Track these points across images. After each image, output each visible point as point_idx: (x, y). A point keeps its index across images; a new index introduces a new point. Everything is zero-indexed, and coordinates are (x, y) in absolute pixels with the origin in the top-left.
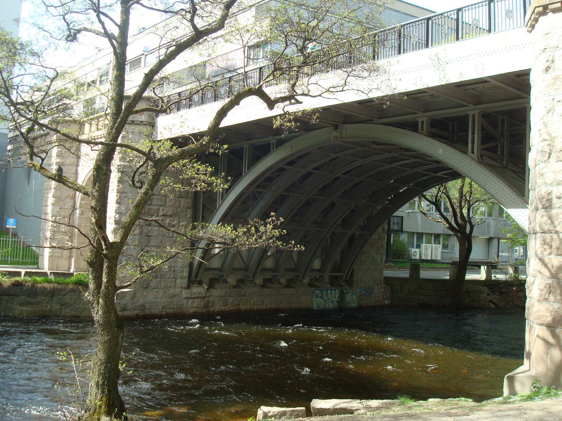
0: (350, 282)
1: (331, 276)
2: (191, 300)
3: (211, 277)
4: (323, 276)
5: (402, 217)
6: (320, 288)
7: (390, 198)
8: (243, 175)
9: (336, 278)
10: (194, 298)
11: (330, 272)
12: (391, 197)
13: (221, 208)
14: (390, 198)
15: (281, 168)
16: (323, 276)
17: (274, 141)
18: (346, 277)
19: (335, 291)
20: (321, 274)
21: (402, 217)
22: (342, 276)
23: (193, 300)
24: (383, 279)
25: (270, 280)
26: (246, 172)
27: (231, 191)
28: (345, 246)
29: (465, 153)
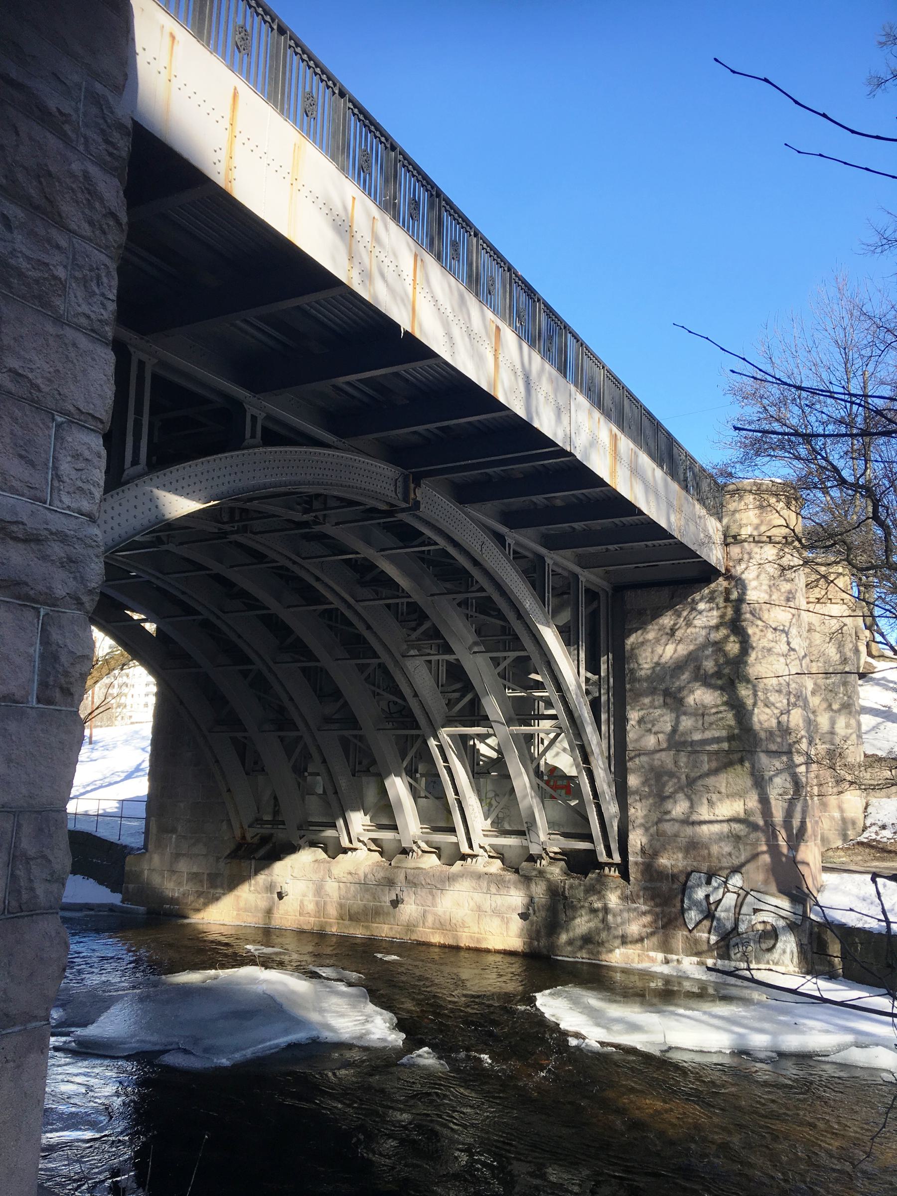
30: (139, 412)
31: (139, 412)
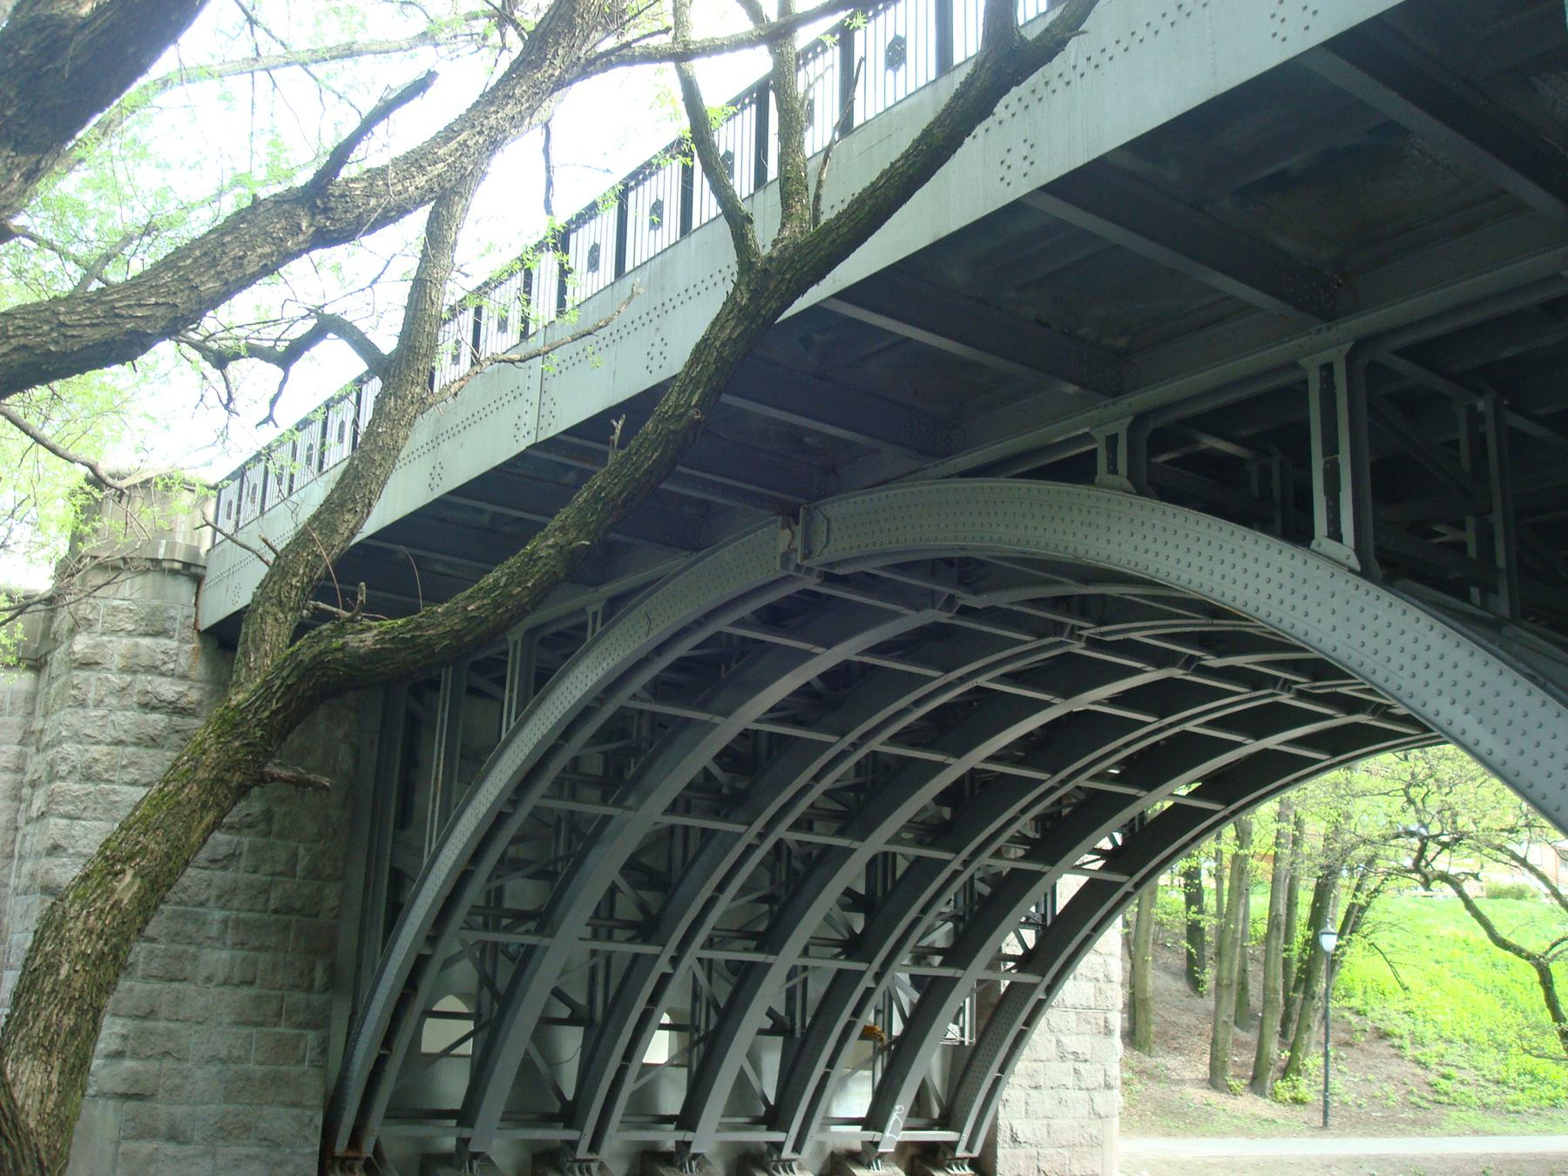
17: (598, 607)
18: (969, 1148)
22: (953, 1146)
30: (1331, 448)
31: (1331, 448)
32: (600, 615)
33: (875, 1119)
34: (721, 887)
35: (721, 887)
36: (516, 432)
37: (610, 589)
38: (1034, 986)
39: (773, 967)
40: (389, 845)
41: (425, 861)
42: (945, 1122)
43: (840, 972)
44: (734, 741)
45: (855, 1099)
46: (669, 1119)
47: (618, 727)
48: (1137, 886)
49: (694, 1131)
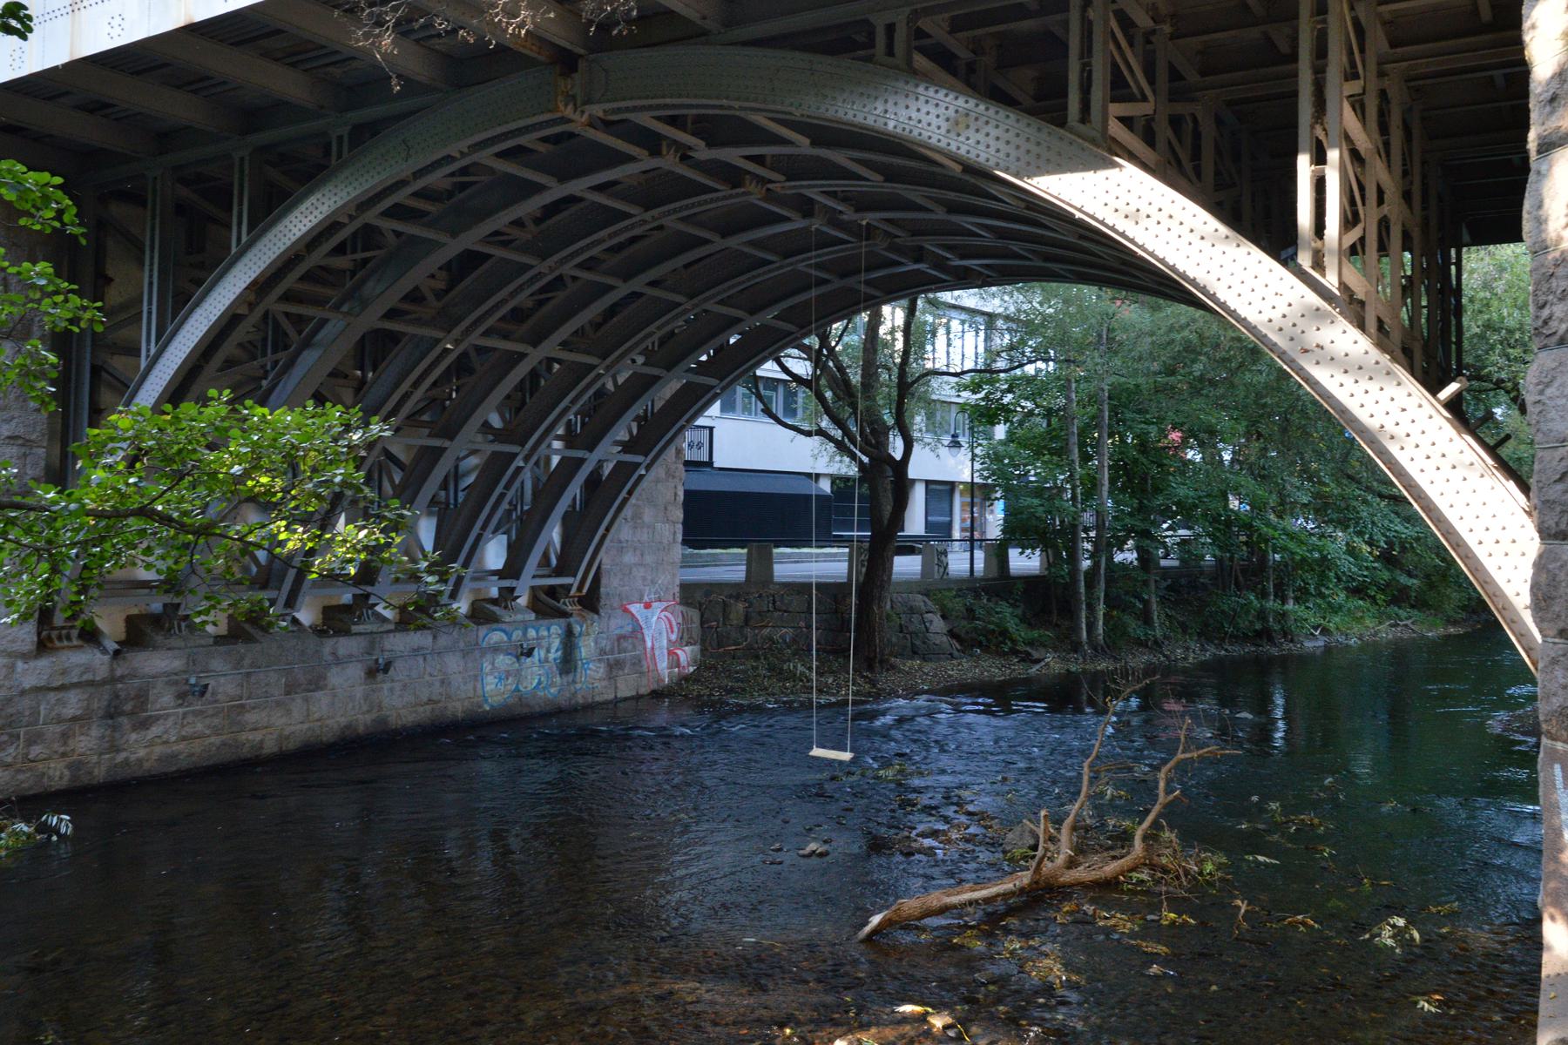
0: (591, 602)
1: (533, 588)
2: (52, 694)
3: (135, 611)
4: (512, 590)
5: (711, 429)
6: (503, 626)
7: (704, 358)
8: (234, 250)
9: (552, 591)
10: (62, 688)
11: (534, 577)
12: (709, 355)
13: (155, 372)
14: (704, 358)
15: (377, 331)
16: (512, 590)
17: (345, 131)
18: (580, 588)
19: (549, 630)
20: (507, 583)
21: (711, 429)
22: (568, 588)
23: (60, 695)
24: (677, 589)
25: (156, 621)
26: (244, 239)
27: (191, 311)
28: (574, 499)
29: (1061, 122)
32: (346, 139)
33: (512, 569)
34: (416, 385)
35: (416, 385)
36: (110, 30)
37: (356, 116)
38: (638, 465)
39: (448, 451)
40: (88, 349)
41: (143, 364)
42: (559, 572)
43: (494, 453)
44: (1296, 83)
45: (494, 554)
46: (494, 573)
47: (368, 236)
48: (723, 389)
49: (518, 579)
